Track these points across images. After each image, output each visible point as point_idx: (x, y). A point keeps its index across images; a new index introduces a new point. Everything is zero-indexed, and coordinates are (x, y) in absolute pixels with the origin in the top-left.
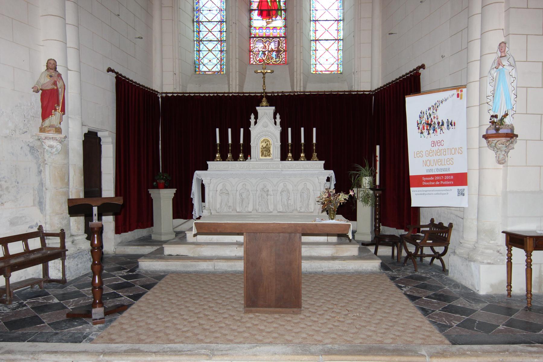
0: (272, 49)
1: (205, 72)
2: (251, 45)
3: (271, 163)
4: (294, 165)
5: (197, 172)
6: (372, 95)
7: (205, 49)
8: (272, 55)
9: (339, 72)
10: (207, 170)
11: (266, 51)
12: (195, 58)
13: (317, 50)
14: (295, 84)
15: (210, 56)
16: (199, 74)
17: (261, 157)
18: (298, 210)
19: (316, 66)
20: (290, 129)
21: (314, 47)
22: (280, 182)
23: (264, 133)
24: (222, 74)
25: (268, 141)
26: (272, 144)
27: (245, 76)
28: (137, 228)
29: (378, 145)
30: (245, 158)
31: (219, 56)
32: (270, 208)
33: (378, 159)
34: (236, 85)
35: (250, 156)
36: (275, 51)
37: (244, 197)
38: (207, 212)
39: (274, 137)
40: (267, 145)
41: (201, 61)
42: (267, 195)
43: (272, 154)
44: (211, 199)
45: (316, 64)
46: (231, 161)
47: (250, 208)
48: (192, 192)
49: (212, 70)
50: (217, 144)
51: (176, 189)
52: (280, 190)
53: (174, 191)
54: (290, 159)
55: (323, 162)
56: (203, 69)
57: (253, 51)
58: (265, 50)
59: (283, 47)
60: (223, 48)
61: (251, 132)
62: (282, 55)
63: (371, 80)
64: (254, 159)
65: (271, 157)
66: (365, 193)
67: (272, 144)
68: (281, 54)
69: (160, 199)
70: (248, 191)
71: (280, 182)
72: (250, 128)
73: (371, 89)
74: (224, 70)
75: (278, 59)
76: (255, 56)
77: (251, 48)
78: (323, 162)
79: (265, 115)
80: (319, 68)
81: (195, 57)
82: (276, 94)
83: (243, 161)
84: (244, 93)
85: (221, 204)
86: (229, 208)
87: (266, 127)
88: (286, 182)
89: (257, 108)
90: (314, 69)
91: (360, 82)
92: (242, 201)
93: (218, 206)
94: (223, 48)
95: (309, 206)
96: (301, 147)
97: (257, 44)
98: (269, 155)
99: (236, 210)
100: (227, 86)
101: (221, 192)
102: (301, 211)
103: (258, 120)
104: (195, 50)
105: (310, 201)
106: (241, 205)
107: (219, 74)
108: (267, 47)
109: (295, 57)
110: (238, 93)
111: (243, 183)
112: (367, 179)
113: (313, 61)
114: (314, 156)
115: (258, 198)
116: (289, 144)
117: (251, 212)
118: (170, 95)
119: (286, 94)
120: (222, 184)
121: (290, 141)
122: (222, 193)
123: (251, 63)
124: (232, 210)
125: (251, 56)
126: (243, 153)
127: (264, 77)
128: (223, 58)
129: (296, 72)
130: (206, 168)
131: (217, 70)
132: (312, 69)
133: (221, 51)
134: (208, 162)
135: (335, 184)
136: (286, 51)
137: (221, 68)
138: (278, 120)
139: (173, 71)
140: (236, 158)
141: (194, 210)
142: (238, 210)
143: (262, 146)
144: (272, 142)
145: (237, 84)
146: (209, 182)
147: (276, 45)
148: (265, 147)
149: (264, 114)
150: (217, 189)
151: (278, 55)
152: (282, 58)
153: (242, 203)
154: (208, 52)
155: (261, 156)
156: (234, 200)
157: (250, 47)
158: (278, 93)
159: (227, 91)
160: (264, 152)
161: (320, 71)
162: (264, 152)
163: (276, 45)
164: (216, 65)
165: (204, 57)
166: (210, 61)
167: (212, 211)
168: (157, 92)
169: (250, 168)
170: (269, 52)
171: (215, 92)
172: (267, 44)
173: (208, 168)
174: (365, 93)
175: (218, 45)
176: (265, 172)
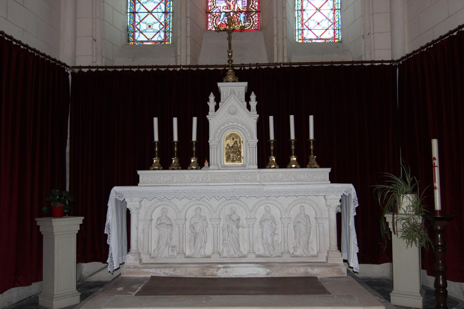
0: (239, 9)
1: (142, 42)
2: (209, 4)
3: (242, 172)
4: (280, 175)
5: (116, 190)
6: (395, 66)
7: (143, 10)
8: (239, 17)
9: (336, 41)
10: (137, 185)
11: (230, 12)
12: (129, 23)
13: (304, 10)
14: (275, 53)
15: (150, 20)
16: (134, 44)
17: (225, 162)
18: (291, 253)
19: (303, 33)
20: (271, 118)
21: (299, 6)
22: (259, 204)
23: (231, 124)
24: (167, 45)
25: (237, 137)
26: (244, 142)
27: (201, 46)
28: (13, 286)
29: (434, 138)
30: (200, 165)
31: (162, 20)
32: (242, 249)
33: (436, 162)
34: (186, 56)
35: (209, 162)
36: (243, 11)
37: (198, 231)
38: (133, 258)
39: (246, 130)
40: (236, 142)
41: (137, 26)
42: (238, 227)
43: (245, 158)
44: (141, 235)
45: (302, 30)
46: (178, 169)
47: (208, 250)
48: (106, 224)
49: (153, 39)
50: (155, 142)
51: (83, 218)
52: (259, 217)
53: (79, 220)
54: (294, 166)
55: (329, 170)
56: (140, 37)
57: (212, 12)
58: (228, 11)
59: (255, 6)
60: (169, 8)
61: (210, 121)
62: (253, 17)
63: (391, 46)
64: (214, 165)
65: (242, 163)
66: (408, 222)
67: (244, 142)
68: (252, 17)
69: (54, 235)
70: (205, 220)
71: (259, 204)
72: (207, 116)
73: (392, 56)
74: (171, 39)
75: (248, 23)
76: (215, 19)
77: (209, 8)
78: (329, 170)
79: (232, 94)
80: (308, 35)
81: (128, 21)
82: (247, 68)
83: (196, 169)
84: (198, 66)
85: (158, 242)
86: (172, 250)
87: (233, 114)
88: (268, 205)
89: (219, 84)
90: (299, 36)
91: (374, 50)
92: (195, 238)
93: (154, 247)
94: (168, 9)
95: (309, 246)
96: (291, 147)
97: (218, 3)
98: (240, 160)
99: (185, 254)
100: (173, 59)
101: (159, 223)
102: (296, 254)
103: (220, 104)
104: (129, 11)
105: (311, 237)
106: (192, 244)
107: (163, 45)
108: (232, 7)
109: (275, 15)
110: (189, 66)
111: (196, 206)
112: (411, 198)
113: (298, 26)
114: (311, 160)
115: (221, 232)
116: (271, 141)
117: (209, 257)
118: (85, 70)
119: (263, 67)
120: (162, 207)
121: (272, 137)
122: (159, 225)
123: (209, 29)
124: (178, 254)
125: (209, 20)
126: (197, 156)
127: (229, 39)
128: (168, 23)
129: (277, 36)
130: (135, 181)
131: (159, 39)
132: (297, 37)
133: (166, 13)
134: (139, 172)
135: (357, 208)
136: (260, 12)
137: (165, 36)
138: (253, 103)
139: (93, 37)
140: (185, 165)
141: (109, 255)
142: (188, 253)
143: (228, 145)
144: (244, 138)
145: (189, 54)
146: (138, 206)
147: (245, 4)
148: (232, 147)
149: (231, 94)
150: (153, 218)
151: (247, 17)
152: (253, 22)
153: (195, 241)
154: (147, 14)
155: (227, 161)
156: (181, 237)
157: (207, 6)
158: (250, 65)
159: (173, 64)
160: (232, 155)
161: (309, 40)
162: (232, 155)
163: (245, 4)
164: (159, 32)
165: (141, 21)
166: (150, 26)
167: (143, 256)
168: (64, 64)
169: (208, 181)
170: (236, 13)
171: (155, 65)
172: (231, 2)
173: (138, 182)
174: (384, 64)
175: (161, 4)
176: (235, 187)
